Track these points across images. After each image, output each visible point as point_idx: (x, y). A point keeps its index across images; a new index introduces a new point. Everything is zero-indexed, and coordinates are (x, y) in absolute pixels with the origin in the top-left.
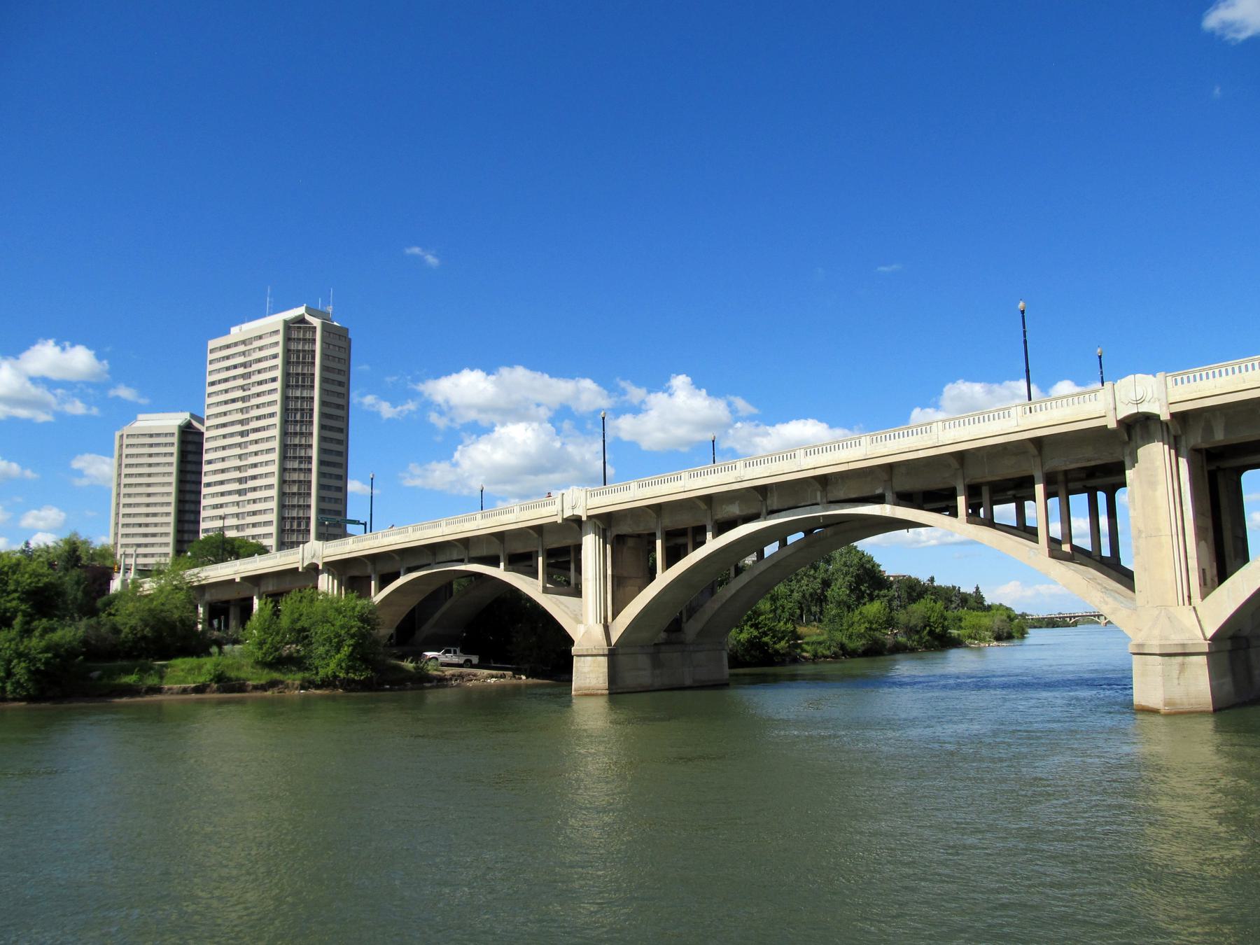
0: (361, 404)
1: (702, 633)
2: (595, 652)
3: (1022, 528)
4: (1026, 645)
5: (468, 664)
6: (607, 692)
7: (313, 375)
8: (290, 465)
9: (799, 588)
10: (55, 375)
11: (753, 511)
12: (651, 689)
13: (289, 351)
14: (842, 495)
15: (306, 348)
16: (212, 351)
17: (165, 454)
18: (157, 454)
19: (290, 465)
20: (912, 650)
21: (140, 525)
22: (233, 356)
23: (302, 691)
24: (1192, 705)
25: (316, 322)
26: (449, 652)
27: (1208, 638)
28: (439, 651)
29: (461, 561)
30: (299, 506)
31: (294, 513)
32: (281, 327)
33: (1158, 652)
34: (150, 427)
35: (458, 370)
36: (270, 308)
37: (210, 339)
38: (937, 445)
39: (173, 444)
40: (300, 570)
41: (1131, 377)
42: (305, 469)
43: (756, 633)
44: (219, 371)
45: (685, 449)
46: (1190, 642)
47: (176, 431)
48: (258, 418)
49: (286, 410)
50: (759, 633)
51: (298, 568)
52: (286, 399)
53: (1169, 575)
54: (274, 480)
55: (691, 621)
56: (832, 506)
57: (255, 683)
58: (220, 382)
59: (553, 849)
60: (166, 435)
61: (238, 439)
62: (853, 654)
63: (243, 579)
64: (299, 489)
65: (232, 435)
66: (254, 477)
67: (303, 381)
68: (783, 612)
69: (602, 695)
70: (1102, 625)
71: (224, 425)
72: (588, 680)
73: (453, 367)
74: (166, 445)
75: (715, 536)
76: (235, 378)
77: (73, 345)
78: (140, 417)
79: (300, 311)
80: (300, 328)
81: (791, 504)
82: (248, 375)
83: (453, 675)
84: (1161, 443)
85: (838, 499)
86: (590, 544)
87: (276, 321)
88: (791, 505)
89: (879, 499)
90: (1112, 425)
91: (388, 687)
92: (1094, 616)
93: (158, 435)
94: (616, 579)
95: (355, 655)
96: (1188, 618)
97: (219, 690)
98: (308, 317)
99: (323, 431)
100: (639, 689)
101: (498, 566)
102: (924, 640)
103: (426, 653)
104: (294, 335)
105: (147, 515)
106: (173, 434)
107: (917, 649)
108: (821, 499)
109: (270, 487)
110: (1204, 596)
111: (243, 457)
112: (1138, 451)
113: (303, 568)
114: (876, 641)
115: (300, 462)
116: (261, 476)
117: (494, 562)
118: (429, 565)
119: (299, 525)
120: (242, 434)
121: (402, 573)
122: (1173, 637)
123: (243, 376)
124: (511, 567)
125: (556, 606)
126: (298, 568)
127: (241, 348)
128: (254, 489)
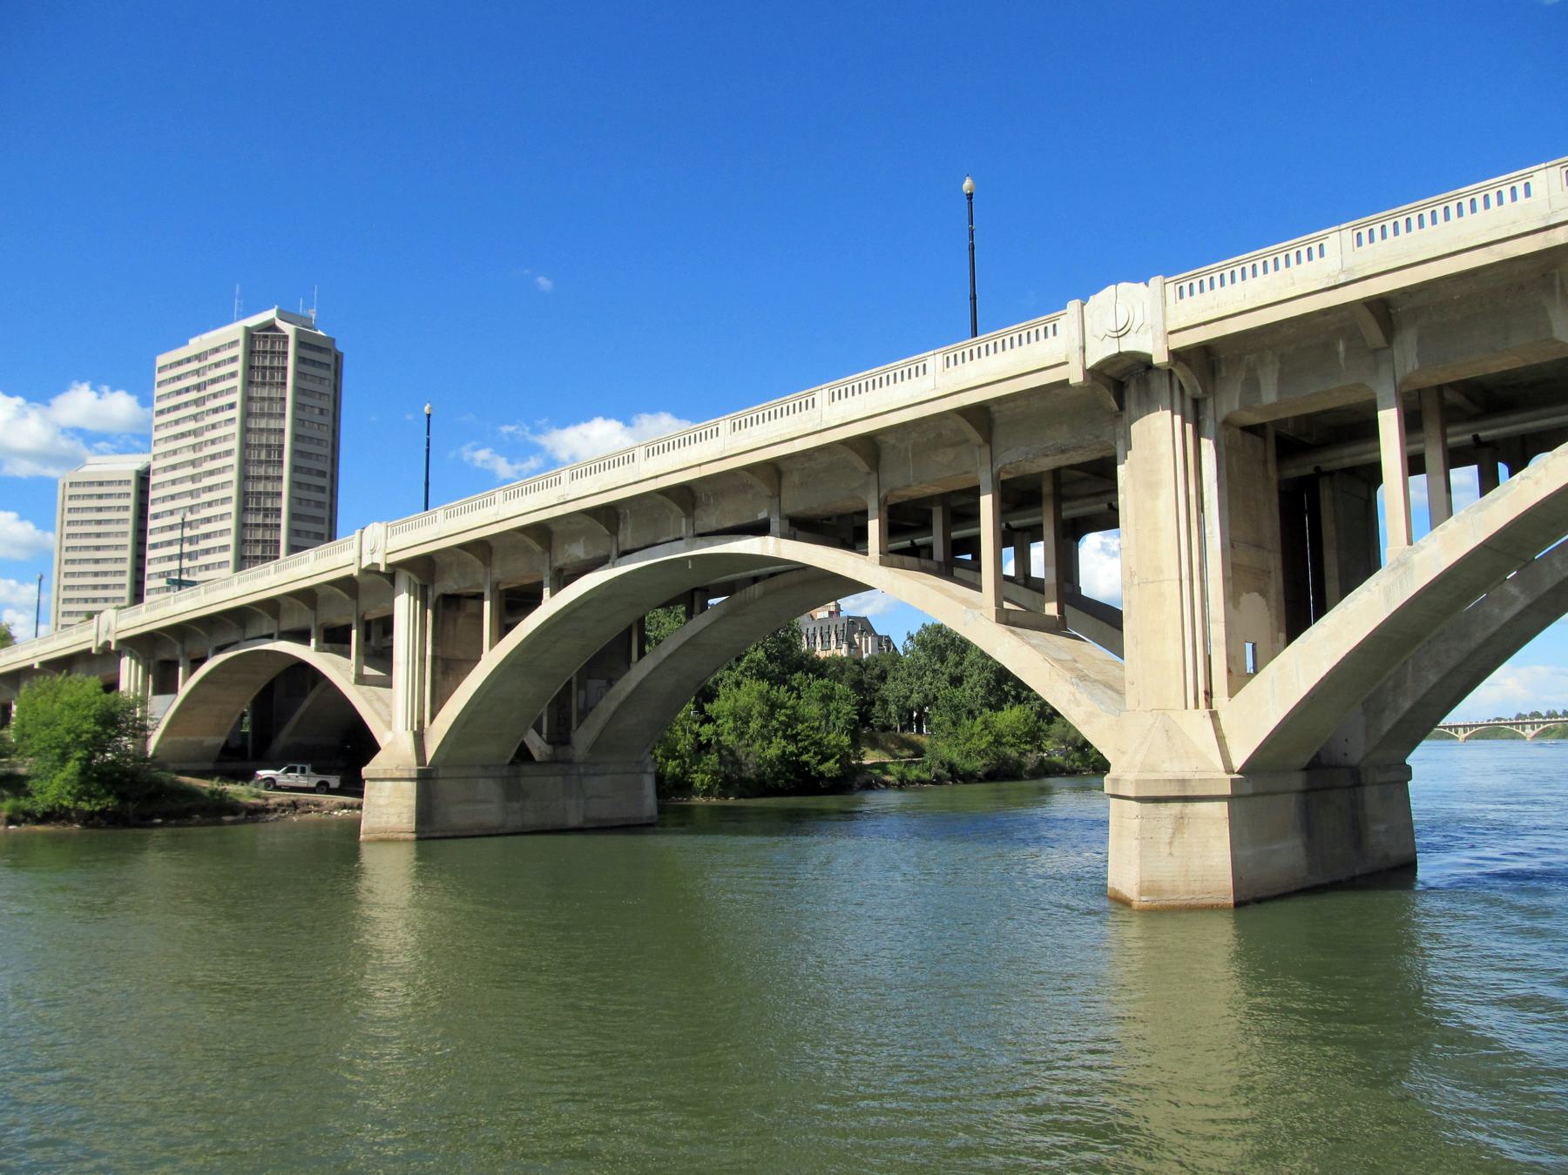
0: (472, 460)
1: (595, 747)
2: (397, 774)
3: (1022, 581)
5: (323, 788)
6: (414, 836)
8: (252, 519)
9: (920, 687)
10: (90, 426)
11: (601, 552)
12: (499, 832)
13: (252, 367)
14: (713, 523)
16: (162, 369)
17: (119, 508)
18: (109, 508)
19: (252, 519)
20: (1072, 773)
21: (86, 600)
22: (186, 375)
23: (11, 827)
24: (1194, 892)
25: (288, 329)
26: (293, 770)
27: (1236, 770)
28: (277, 769)
29: (270, 637)
32: (241, 336)
33: (1132, 794)
34: (99, 472)
35: (587, 418)
36: (238, 313)
38: (819, 429)
39: (128, 494)
40: (94, 651)
41: (1111, 289)
42: (271, 525)
43: (792, 748)
44: (169, 395)
46: (1197, 776)
47: (132, 478)
50: (798, 749)
53: (1172, 652)
54: (230, 540)
55: (581, 728)
56: (699, 541)
58: (169, 410)
60: (120, 483)
61: (188, 486)
62: (969, 777)
63: (43, 664)
64: (263, 551)
66: (207, 536)
68: (838, 718)
69: (406, 840)
70: (1528, 739)
71: (174, 467)
72: (385, 818)
73: (583, 415)
74: (119, 496)
75: (552, 594)
76: (186, 404)
77: (113, 390)
79: (270, 315)
80: (266, 337)
81: (649, 540)
83: (280, 805)
84: (1169, 412)
85: (708, 530)
86: (403, 607)
87: (235, 331)
88: (648, 541)
89: (761, 529)
90: (1076, 377)
91: (159, 821)
93: (110, 483)
94: (439, 663)
95: (89, 773)
96: (1198, 723)
98: (280, 324)
100: (477, 832)
101: (308, 643)
102: (1092, 760)
103: (259, 772)
105: (95, 587)
106: (129, 481)
107: (1081, 772)
108: (687, 532)
109: (225, 548)
110: (1232, 693)
112: (1132, 427)
113: (98, 649)
114: (1005, 760)
115: (266, 516)
117: (302, 636)
121: (210, 653)
122: (1166, 766)
123: (197, 402)
124: (327, 646)
125: (362, 700)
127: (195, 365)
128: (207, 552)
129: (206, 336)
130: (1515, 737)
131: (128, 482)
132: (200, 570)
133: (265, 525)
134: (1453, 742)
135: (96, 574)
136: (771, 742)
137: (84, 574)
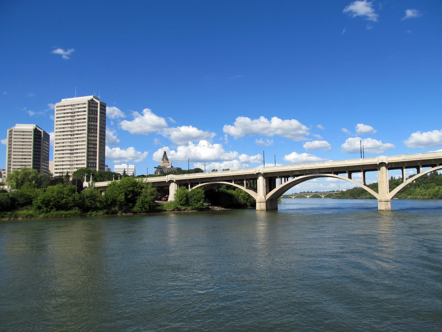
7: (97, 118)
8: (90, 146)
15: (95, 109)
19: (90, 146)
25: (98, 102)
29: (220, 181)
30: (93, 159)
31: (92, 161)
34: (23, 129)
45: (147, 135)
48: (78, 130)
49: (89, 129)
51: (166, 181)
52: (89, 125)
57: (183, 209)
60: (29, 132)
61: (70, 137)
65: (67, 135)
67: (94, 120)
71: (63, 132)
73: (289, 153)
76: (67, 117)
78: (17, 125)
82: (74, 124)
90: (378, 164)
92: (291, 195)
93: (26, 132)
97: (177, 211)
98: (94, 99)
101: (232, 183)
104: (91, 105)
111: (72, 142)
116: (80, 149)
118: (209, 182)
119: (93, 165)
120: (71, 135)
125: (251, 192)
126: (166, 181)
127: (70, 107)
129: (68, 99)
130: (290, 198)
131: (31, 132)
132: (74, 157)
133: (93, 148)
134: (306, 199)
135: (22, 155)
136: (433, 195)
137: (19, 155)
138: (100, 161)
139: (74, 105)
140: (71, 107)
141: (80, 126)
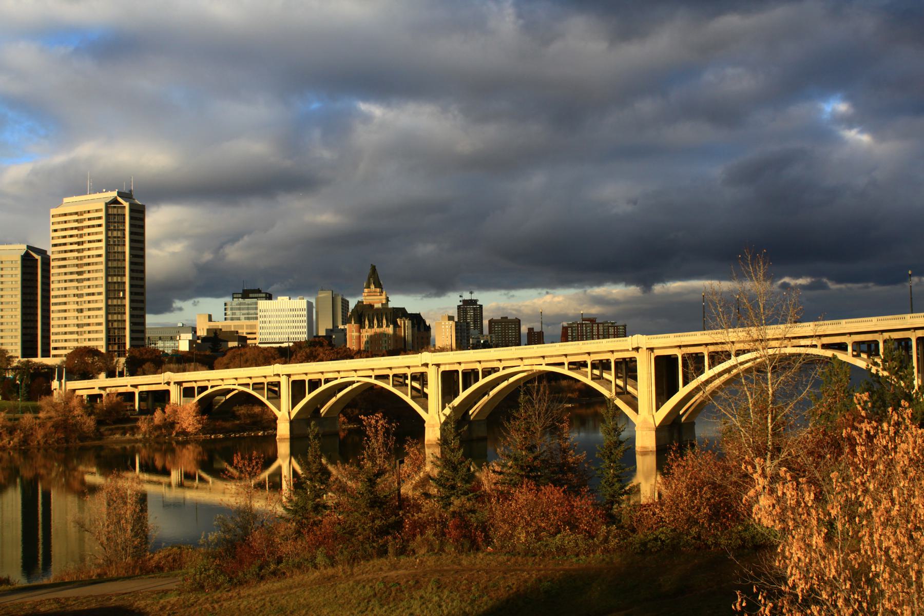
4: (657, 475)
37: (53, 208)
49: (108, 291)
59: (813, 607)
82: (82, 228)
99: (133, 266)
127: (76, 217)
138: (133, 257)
139: (82, 213)
140: (77, 230)
141: (93, 234)
